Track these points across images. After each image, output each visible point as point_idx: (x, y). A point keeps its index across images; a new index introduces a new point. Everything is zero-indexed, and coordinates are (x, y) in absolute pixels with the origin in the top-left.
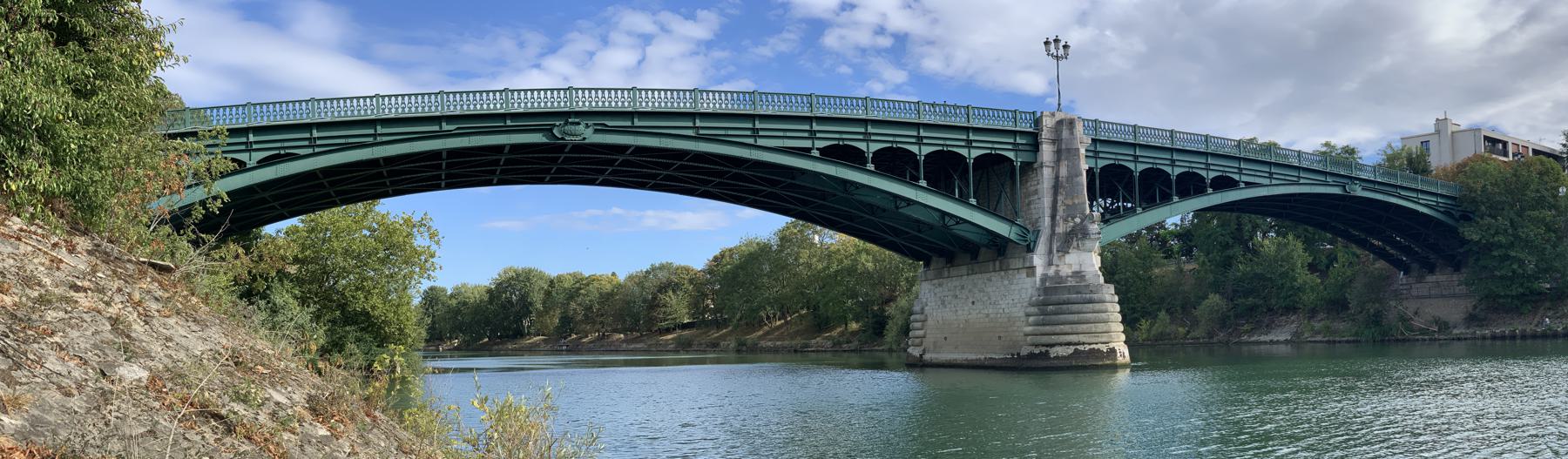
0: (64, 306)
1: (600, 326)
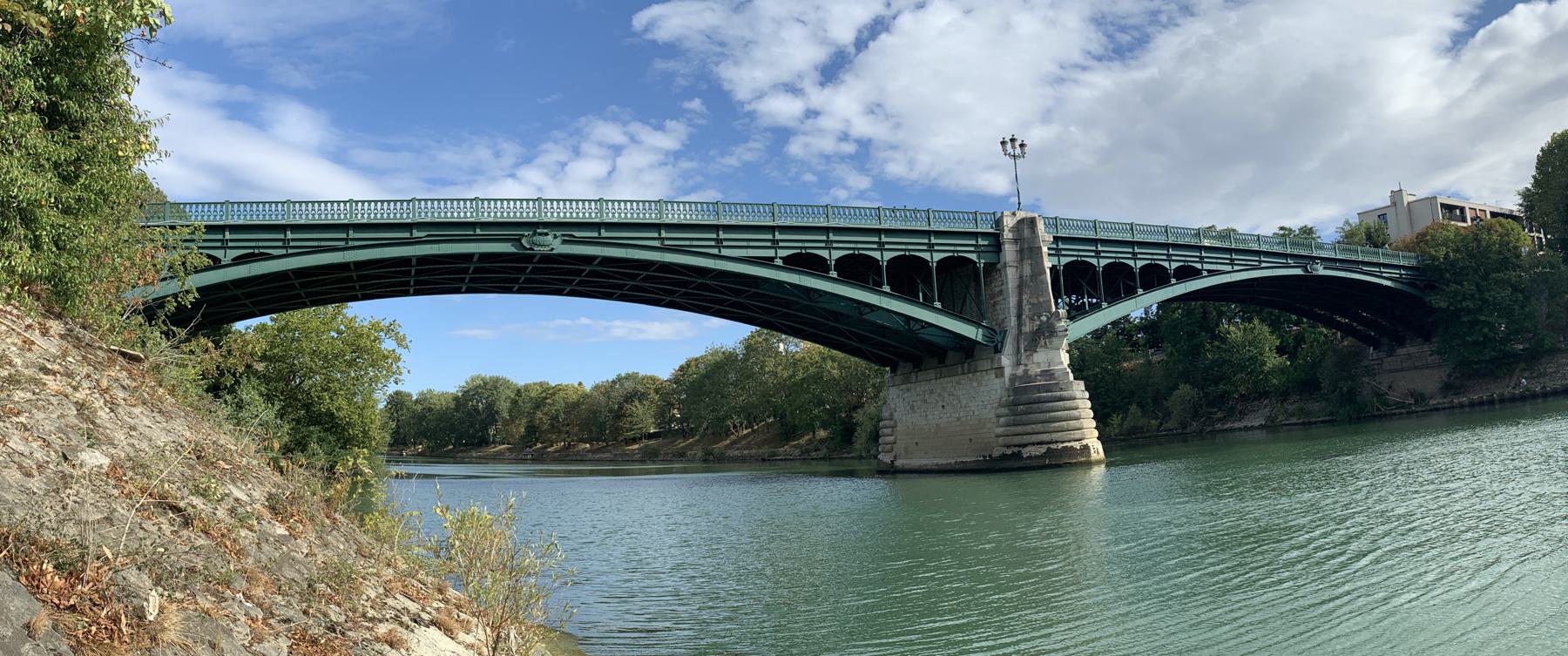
0: (33, 387)
1: (566, 436)
